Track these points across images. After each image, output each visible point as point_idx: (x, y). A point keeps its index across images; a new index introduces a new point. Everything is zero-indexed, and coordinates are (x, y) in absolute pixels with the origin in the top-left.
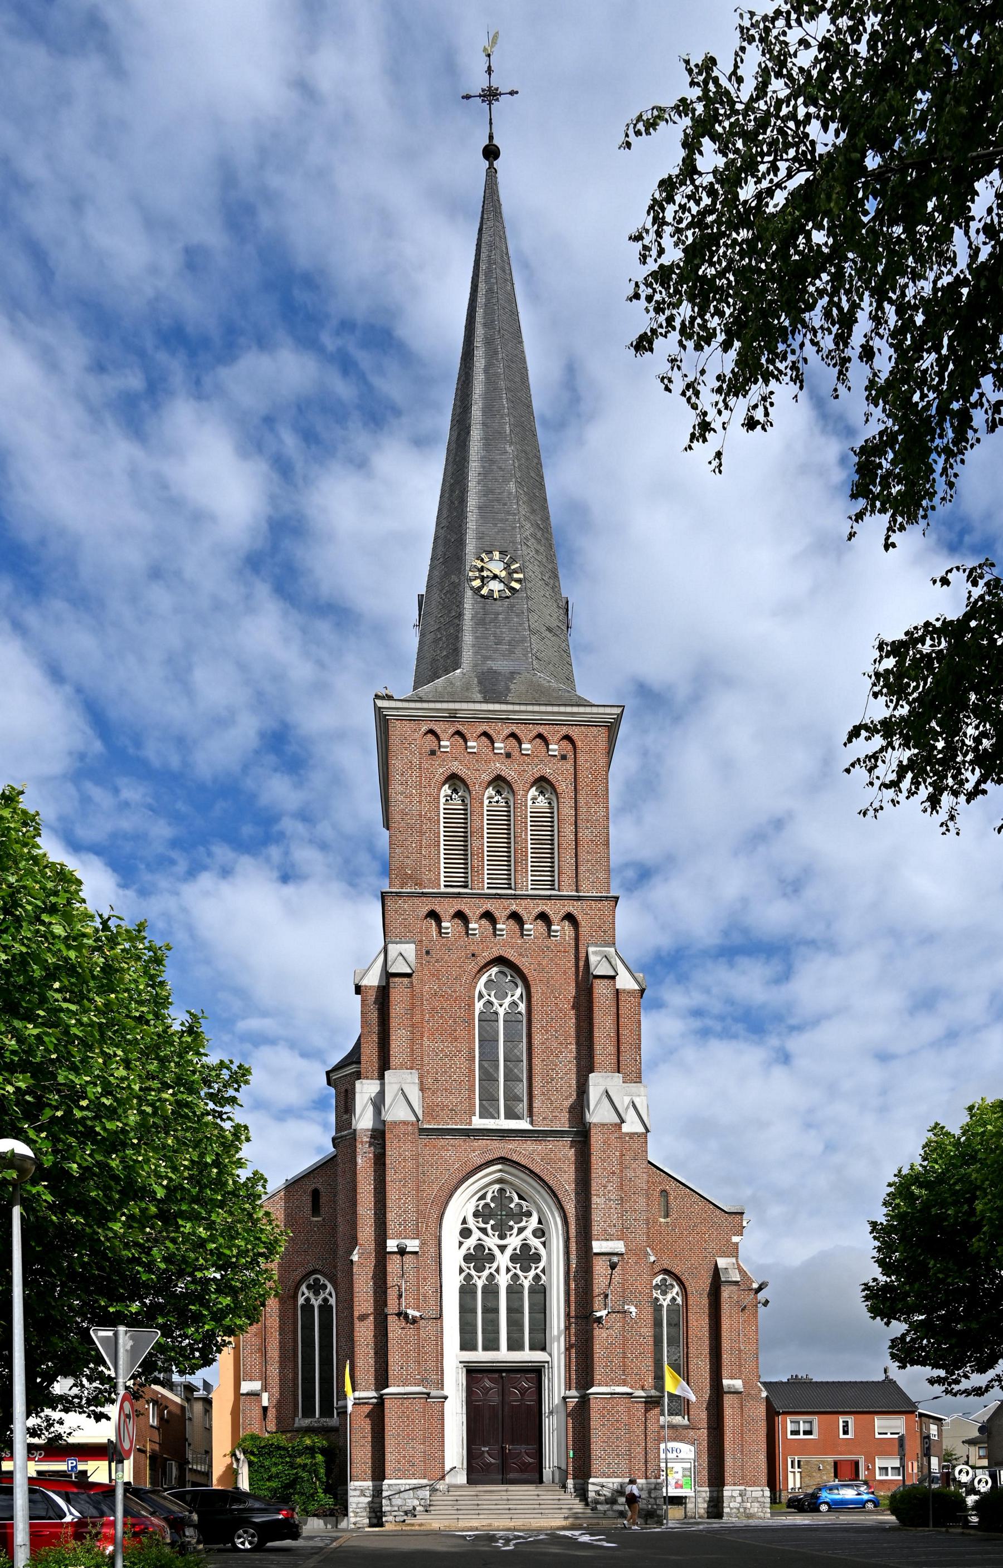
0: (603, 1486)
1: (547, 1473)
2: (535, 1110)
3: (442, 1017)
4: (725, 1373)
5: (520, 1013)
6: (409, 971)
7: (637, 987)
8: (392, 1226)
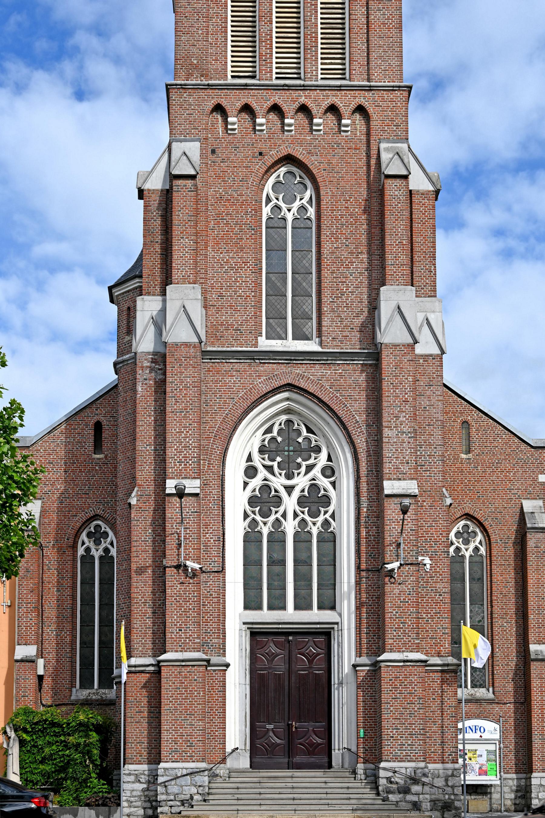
0: (395, 772)
1: (336, 754)
2: (324, 329)
3: (227, 224)
4: (532, 636)
5: (309, 219)
6: (193, 172)
7: (431, 188)
8: (172, 465)
